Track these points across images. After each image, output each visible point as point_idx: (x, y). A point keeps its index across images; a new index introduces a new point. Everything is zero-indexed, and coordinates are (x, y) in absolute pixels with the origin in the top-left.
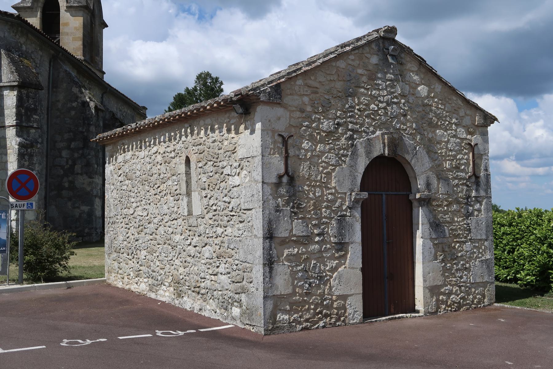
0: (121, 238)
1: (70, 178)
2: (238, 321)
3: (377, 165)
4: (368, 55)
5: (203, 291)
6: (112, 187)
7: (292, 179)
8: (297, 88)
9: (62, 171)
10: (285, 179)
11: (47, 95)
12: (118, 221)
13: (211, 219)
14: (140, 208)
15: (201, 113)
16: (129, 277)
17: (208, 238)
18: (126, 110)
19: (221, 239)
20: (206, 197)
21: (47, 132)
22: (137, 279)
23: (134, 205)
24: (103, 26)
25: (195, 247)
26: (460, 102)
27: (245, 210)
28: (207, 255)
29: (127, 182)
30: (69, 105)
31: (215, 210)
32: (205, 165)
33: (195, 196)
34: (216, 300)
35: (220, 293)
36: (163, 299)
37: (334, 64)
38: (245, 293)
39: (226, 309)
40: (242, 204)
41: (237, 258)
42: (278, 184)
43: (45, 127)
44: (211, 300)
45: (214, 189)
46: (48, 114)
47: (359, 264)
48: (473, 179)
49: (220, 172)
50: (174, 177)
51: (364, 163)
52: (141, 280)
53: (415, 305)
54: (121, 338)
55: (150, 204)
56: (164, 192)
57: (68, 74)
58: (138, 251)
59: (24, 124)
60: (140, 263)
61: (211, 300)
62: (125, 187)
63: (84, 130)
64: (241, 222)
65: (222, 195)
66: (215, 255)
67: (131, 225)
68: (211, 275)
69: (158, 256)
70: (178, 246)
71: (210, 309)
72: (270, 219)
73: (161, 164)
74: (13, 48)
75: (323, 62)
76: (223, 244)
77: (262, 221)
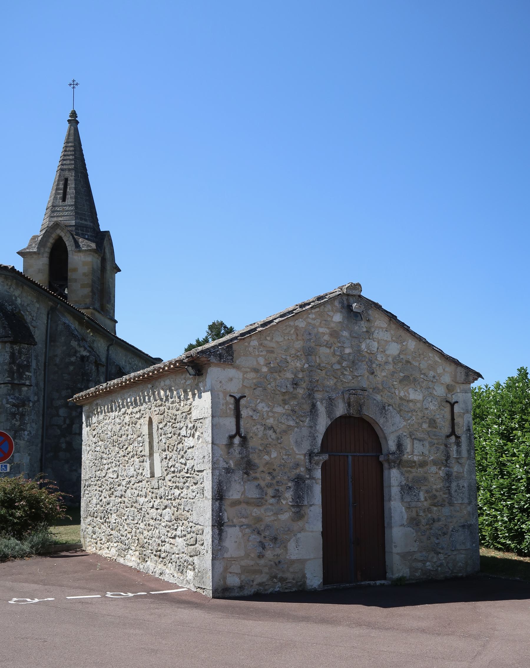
0: (94, 501)
1: (68, 439)
2: (192, 585)
3: (338, 426)
4: (331, 313)
5: (163, 555)
6: (88, 448)
7: (244, 440)
8: (251, 349)
9: (58, 431)
10: (237, 440)
11: (44, 350)
12: (92, 483)
13: (170, 481)
14: (111, 470)
15: (161, 374)
16: (101, 542)
17: (167, 500)
18: (136, 362)
19: (179, 501)
20: (166, 458)
21: (44, 389)
22: (108, 544)
23: (106, 467)
24: (115, 270)
25: (157, 509)
26: (437, 359)
27: (198, 471)
28: (167, 518)
29: (100, 443)
30: (67, 360)
31: (174, 472)
32: (164, 427)
33: (157, 457)
34: (174, 563)
35: (177, 556)
36: (130, 564)
37: (292, 323)
38: (197, 555)
39: (182, 573)
40: (195, 465)
41: (191, 520)
42: (230, 444)
43: (42, 384)
44: (170, 564)
45: (173, 450)
46: (45, 370)
47: (319, 527)
48: (453, 438)
49: (178, 433)
50: (140, 439)
51: (325, 423)
52: (112, 545)
53: (386, 573)
54: (68, 598)
55: (119, 466)
56: (132, 454)
57: (68, 327)
58: (109, 515)
59: (16, 382)
60: (111, 527)
61: (170, 564)
62: (99, 448)
63: (83, 387)
64: (196, 484)
65: (179, 456)
66: (173, 518)
67: (104, 488)
68: (170, 538)
69: (126, 520)
70: (143, 509)
71: (169, 574)
72: (219, 481)
73: (129, 425)
74: (6, 302)
75: (279, 322)
76: (179, 507)
77: (211, 483)
